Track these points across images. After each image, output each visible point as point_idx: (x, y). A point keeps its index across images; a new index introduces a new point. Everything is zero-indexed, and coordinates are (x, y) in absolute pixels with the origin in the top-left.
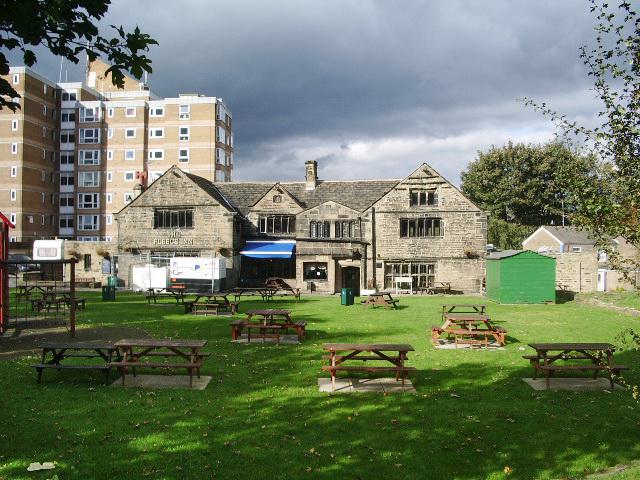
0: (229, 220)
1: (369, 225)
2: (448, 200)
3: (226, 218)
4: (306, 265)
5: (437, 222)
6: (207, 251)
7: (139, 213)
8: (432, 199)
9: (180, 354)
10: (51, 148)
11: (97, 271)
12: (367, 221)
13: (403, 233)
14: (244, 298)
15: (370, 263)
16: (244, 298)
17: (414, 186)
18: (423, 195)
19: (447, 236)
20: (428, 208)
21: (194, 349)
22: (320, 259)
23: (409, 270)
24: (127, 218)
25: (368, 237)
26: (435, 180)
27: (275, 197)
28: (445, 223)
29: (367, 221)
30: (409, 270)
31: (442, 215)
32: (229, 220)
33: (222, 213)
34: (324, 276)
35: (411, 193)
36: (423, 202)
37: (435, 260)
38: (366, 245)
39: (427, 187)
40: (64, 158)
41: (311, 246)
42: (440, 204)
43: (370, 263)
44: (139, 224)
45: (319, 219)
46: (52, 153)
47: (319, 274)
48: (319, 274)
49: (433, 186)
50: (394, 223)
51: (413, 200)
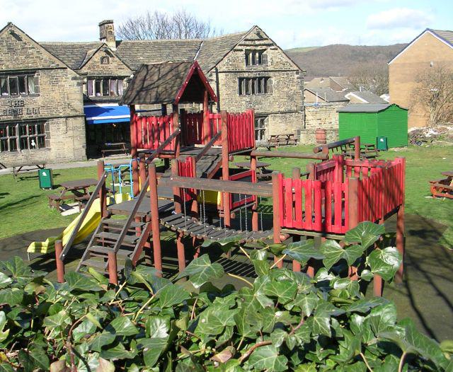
2: (275, 60)
3: (75, 82)
12: (212, 80)
17: (248, 48)
19: (275, 94)
20: (260, 68)
27: (102, 59)
29: (212, 80)
42: (269, 63)
49: (264, 47)
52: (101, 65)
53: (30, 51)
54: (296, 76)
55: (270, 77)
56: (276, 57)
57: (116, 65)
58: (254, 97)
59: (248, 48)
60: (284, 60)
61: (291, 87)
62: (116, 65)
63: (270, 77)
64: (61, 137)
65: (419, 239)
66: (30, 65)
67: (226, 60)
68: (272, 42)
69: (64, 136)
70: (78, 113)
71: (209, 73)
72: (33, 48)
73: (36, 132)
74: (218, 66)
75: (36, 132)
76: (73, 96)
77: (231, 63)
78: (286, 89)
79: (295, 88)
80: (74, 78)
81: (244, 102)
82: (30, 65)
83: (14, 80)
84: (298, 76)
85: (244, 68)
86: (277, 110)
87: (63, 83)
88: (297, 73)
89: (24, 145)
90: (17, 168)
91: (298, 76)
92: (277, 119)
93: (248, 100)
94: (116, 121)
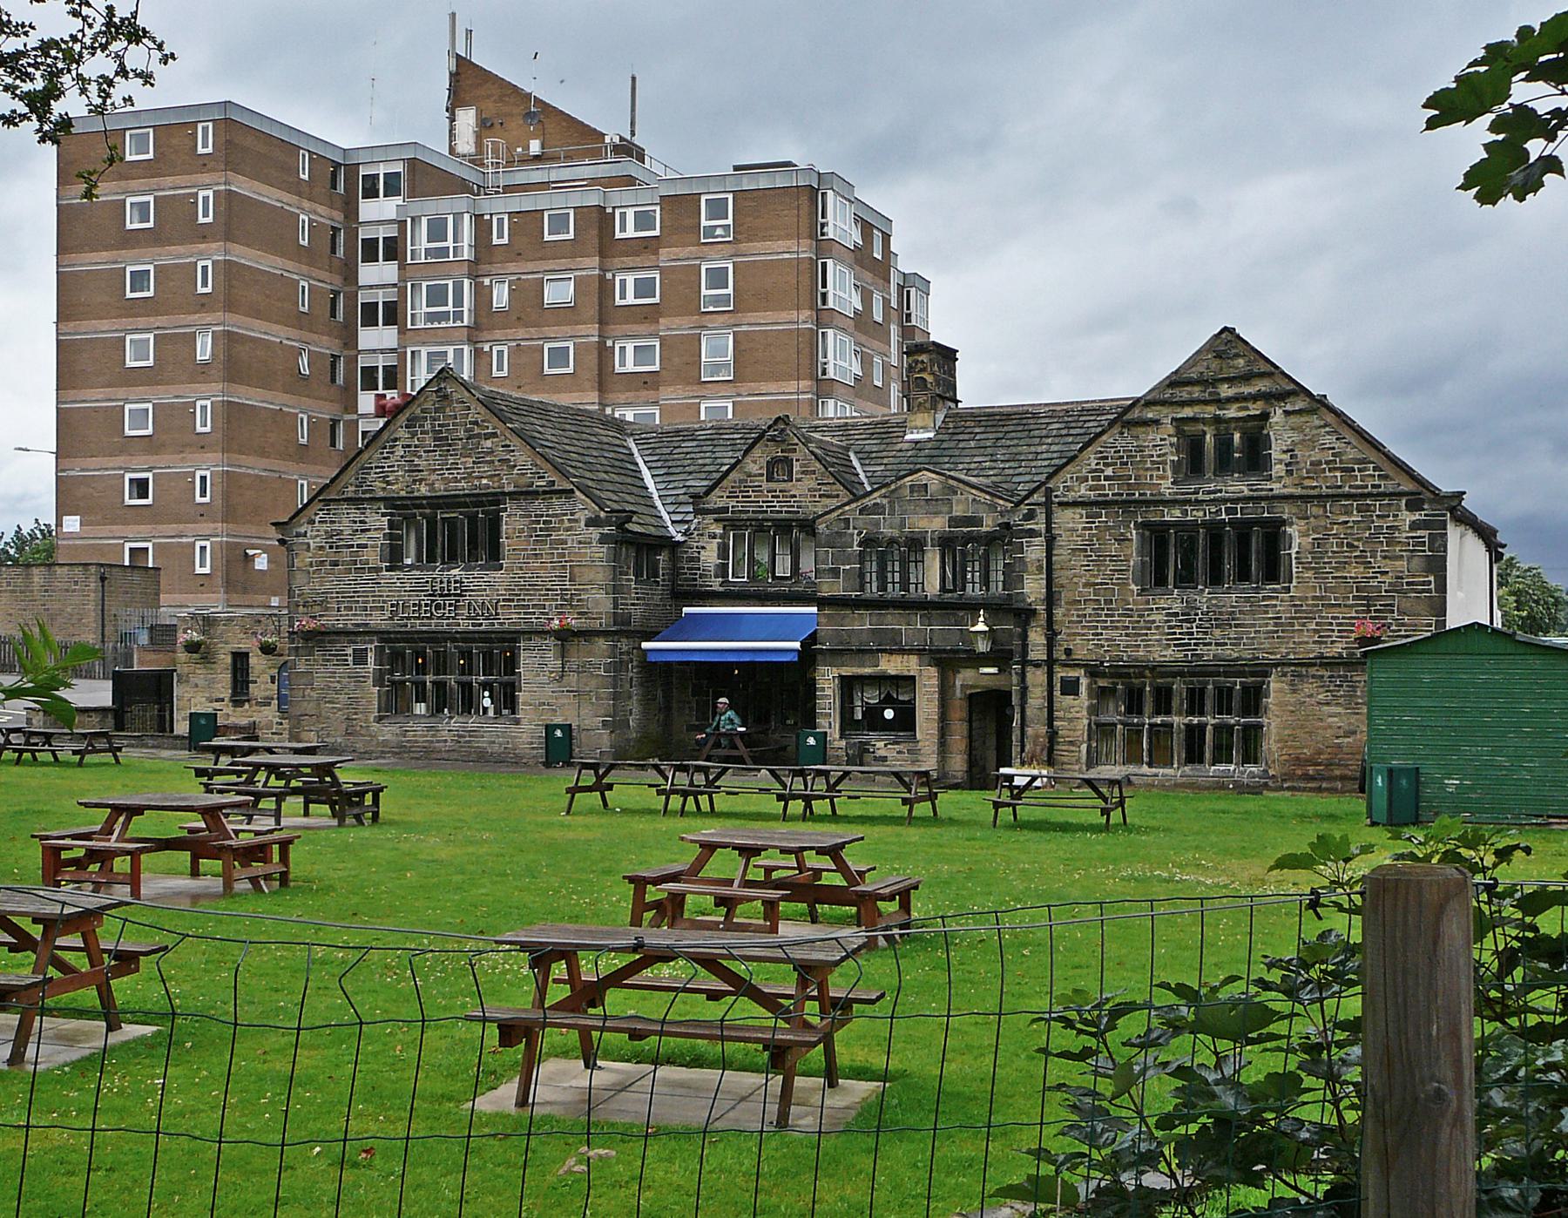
0: (603, 539)
1: (1034, 551)
2: (1306, 456)
3: (595, 533)
4: (848, 685)
5: (1274, 534)
6: (536, 641)
7: (346, 518)
8: (1255, 458)
9: (744, 988)
10: (331, 281)
11: (266, 703)
12: (1032, 533)
13: (1155, 577)
14: (1309, 785)
15: (1036, 677)
16: (1309, 785)
17: (1187, 412)
18: (1224, 444)
19: (1301, 583)
20: (1237, 486)
21: (810, 973)
22: (891, 665)
23: (1236, 703)
24: (313, 535)
25: (1033, 588)
26: (1261, 386)
27: (772, 465)
28: (1297, 538)
29: (1032, 533)
30: (1236, 703)
31: (1286, 511)
32: (603, 539)
33: (582, 516)
34: (906, 721)
35: (1179, 433)
36: (1224, 465)
37: (1262, 670)
38: (1025, 615)
39: (1232, 412)
40: (370, 310)
41: (862, 624)
42: (1278, 470)
43: (1036, 677)
44: (345, 556)
45: (887, 531)
46: (336, 293)
47: (889, 714)
48: (889, 714)
49: (1255, 409)
50: (1122, 540)
51: (1192, 462)
52: (765, 485)
53: (488, 443)
54: (1408, 517)
55: (1283, 522)
56: (1311, 443)
57: (813, 484)
58: (1203, 597)
59: (1187, 412)
60: (1351, 454)
61: (1379, 562)
62: (813, 484)
63: (1283, 522)
64: (548, 689)
65: (1018, 1205)
66: (484, 481)
67: (1091, 459)
68: (1292, 386)
69: (555, 686)
70: (596, 625)
71: (1024, 509)
72: (494, 435)
73: (1148, 707)
74: (1058, 484)
75: (1148, 707)
76: (589, 575)
77: (1109, 472)
78: (1354, 571)
79: (1402, 565)
80: (590, 523)
81: (1158, 617)
82: (484, 481)
83: (451, 523)
84: (1416, 516)
85: (1166, 487)
86: (1313, 651)
87: (563, 535)
88: (1413, 506)
89: (469, 704)
90: (27, 755)
91: (1416, 516)
92: (1308, 688)
93: (1177, 607)
94: (747, 658)
